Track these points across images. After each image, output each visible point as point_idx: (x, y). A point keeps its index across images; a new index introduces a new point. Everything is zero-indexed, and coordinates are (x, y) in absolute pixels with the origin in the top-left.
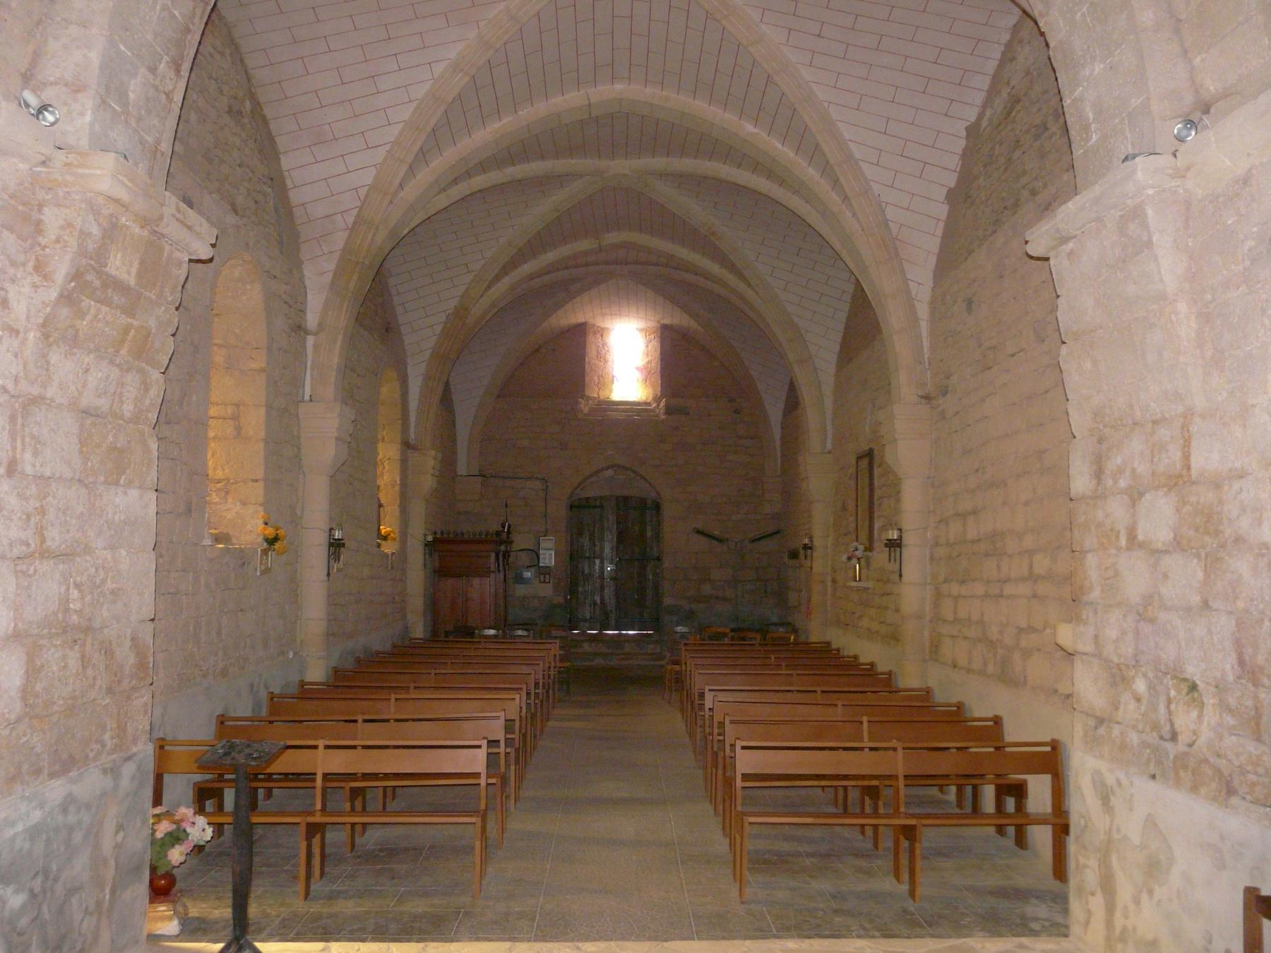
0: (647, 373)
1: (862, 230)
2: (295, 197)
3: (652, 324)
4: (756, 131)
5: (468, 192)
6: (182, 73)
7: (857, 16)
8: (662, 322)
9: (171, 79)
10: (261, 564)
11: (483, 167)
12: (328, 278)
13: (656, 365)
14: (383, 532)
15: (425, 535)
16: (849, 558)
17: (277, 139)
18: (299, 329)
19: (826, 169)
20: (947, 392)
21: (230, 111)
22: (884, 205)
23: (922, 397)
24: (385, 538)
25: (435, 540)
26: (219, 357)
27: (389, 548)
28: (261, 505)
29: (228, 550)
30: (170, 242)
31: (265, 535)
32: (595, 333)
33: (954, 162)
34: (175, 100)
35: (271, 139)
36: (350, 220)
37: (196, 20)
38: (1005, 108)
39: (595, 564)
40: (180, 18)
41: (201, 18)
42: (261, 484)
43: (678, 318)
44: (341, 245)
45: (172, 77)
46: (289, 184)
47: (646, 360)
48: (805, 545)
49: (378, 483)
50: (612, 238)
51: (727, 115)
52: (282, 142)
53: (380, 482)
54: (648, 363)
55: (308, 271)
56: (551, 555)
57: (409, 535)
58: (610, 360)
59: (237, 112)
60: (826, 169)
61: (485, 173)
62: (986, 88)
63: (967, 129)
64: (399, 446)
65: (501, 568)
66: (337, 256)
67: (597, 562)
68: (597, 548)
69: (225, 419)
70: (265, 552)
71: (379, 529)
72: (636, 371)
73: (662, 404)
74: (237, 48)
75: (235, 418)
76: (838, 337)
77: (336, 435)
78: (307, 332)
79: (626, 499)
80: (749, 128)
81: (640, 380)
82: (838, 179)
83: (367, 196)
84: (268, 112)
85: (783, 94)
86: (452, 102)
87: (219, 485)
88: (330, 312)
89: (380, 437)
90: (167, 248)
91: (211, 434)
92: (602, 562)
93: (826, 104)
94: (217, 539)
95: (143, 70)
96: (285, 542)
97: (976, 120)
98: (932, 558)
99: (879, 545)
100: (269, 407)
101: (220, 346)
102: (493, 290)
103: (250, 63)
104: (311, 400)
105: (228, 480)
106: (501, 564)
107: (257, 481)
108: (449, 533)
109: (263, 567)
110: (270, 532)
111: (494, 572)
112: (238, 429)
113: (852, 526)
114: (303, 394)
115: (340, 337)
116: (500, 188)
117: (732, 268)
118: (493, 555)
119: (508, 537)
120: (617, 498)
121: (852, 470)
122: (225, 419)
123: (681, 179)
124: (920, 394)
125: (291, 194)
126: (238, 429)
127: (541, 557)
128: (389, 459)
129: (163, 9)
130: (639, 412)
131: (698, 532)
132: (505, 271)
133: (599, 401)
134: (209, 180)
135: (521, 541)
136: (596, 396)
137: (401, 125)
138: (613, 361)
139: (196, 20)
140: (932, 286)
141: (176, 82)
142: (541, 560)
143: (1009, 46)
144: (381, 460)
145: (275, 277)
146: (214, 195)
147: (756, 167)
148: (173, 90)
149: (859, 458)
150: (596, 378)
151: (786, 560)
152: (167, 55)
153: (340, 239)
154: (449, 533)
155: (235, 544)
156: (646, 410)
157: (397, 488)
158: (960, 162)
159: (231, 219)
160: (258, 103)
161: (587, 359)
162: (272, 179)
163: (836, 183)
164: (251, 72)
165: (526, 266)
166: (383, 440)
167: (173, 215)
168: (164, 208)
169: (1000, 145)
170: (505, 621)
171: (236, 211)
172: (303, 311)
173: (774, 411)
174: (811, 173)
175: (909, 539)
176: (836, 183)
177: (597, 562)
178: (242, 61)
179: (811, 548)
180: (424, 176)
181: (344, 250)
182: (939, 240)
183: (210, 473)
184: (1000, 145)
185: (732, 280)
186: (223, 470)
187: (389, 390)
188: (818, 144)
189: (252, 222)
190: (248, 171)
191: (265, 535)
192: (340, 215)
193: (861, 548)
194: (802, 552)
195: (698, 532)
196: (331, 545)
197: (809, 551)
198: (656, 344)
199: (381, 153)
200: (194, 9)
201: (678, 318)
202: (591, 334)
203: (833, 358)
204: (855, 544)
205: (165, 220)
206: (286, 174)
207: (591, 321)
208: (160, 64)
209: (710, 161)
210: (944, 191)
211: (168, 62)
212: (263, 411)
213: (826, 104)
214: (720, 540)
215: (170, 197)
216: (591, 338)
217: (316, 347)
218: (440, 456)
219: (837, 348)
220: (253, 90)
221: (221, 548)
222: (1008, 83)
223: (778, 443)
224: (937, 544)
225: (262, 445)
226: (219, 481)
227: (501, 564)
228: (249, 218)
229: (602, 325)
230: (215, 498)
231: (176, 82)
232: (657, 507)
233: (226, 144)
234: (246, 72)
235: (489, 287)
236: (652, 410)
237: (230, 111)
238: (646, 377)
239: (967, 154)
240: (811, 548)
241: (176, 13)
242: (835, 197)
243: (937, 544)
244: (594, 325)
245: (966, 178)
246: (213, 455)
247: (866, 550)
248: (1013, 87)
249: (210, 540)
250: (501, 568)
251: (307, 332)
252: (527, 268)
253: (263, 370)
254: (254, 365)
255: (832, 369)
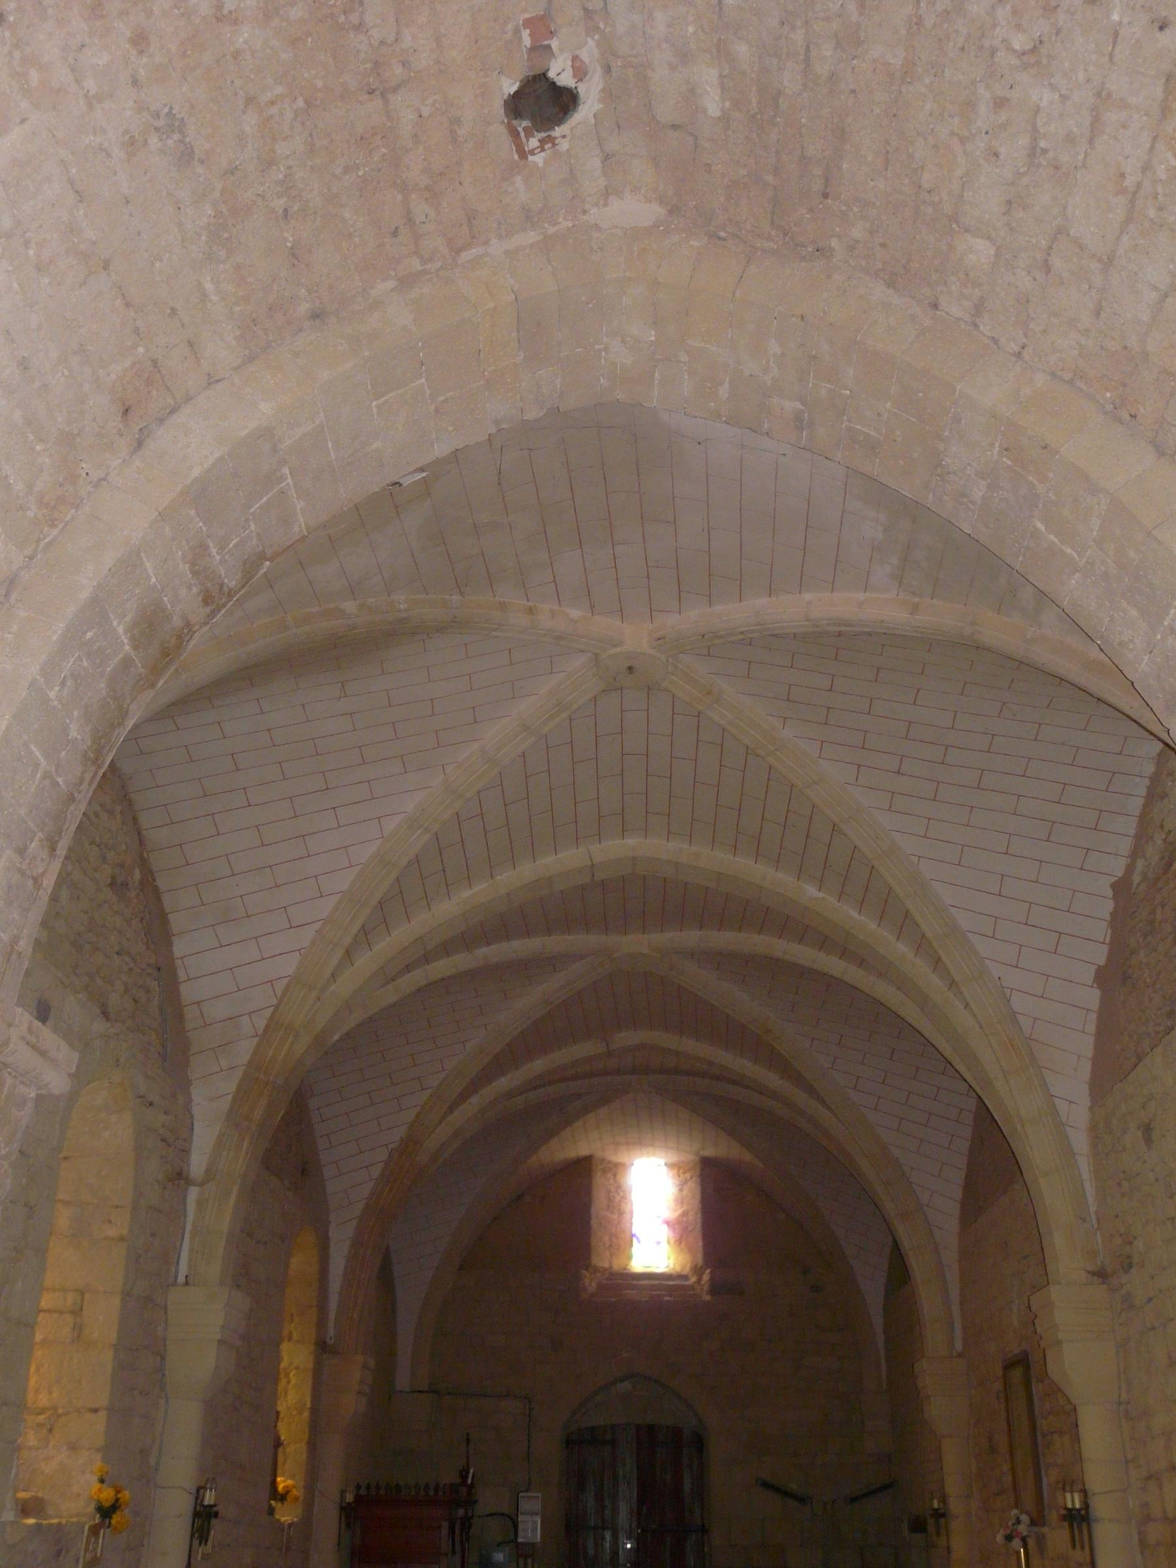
0: (681, 1230)
1: (980, 1028)
2: (187, 992)
3: (688, 1157)
4: (821, 895)
5: (423, 983)
6: (58, 852)
7: (947, 747)
8: (702, 1153)
9: (42, 860)
10: (86, 1550)
11: (447, 948)
12: (225, 1104)
13: (695, 1218)
14: (281, 1487)
15: (343, 1493)
16: (1009, 1538)
17: (171, 917)
18: (179, 1177)
19: (922, 945)
20: (1130, 1266)
21: (112, 885)
22: (1008, 991)
23: (1093, 1274)
24: (282, 1498)
25: (358, 1498)
26: (63, 1219)
27: (286, 1515)
28: (98, 1450)
29: (38, 1526)
30: (13, 1074)
31: (99, 1501)
32: (604, 1171)
33: (1101, 930)
34: (45, 884)
35: (163, 917)
36: (261, 1024)
37: (84, 786)
38: (1162, 858)
39: (603, 1538)
40: (64, 787)
41: (90, 785)
42: (103, 1414)
43: (723, 1148)
44: (245, 1058)
45: (44, 857)
46: (181, 974)
47: (680, 1211)
48: (936, 1510)
49: (279, 1408)
50: (625, 1038)
51: (780, 875)
52: (176, 922)
53: (281, 1407)
54: (684, 1214)
55: (198, 1094)
56: (535, 1522)
57: (317, 1492)
58: (627, 1211)
59: (122, 884)
60: (922, 945)
61: (448, 955)
62: (1132, 832)
63: (1114, 886)
64: (312, 1348)
65: (457, 1548)
66: (238, 1074)
67: (608, 1535)
68: (607, 1512)
69: (61, 1313)
70: (95, 1531)
71: (274, 1483)
72: (665, 1226)
73: (706, 1277)
74: (130, 804)
75: (77, 1311)
76: (959, 1177)
77: (218, 1337)
78: (189, 1182)
79: (651, 1429)
80: (811, 891)
81: (672, 1241)
82: (939, 959)
83: (285, 991)
84: (162, 883)
85: (855, 847)
86: (406, 867)
87: (41, 1418)
88: (225, 1153)
89: (285, 1333)
90: (9, 1081)
91: (38, 1337)
92: (615, 1537)
93: (915, 859)
94: (25, 1509)
95: (9, 852)
96: (127, 1511)
97: (1125, 874)
98: (1143, 1543)
99: (1053, 1516)
100: (126, 1295)
101: (67, 1203)
102: (456, 1113)
103: (144, 820)
104: (187, 1283)
105: (55, 1408)
106: (457, 1544)
107: (96, 1411)
108: (378, 1487)
109: (89, 1556)
110: (107, 1495)
111: (446, 1555)
112: (78, 1330)
113: (1008, 1480)
114: (177, 1272)
115: (235, 1189)
116: (471, 975)
117: (798, 1079)
118: (445, 1524)
119: (469, 1494)
120: (638, 1427)
121: (998, 1386)
122: (61, 1313)
123: (719, 960)
124: (1089, 1268)
125: (184, 989)
126: (78, 1330)
127: (521, 1526)
128: (297, 1368)
129: (44, 778)
130: (671, 1290)
131: (767, 1485)
132: (474, 1086)
133: (611, 1274)
134: (76, 975)
135: (489, 1500)
136: (606, 1265)
137: (337, 898)
138: (631, 1212)
139: (84, 786)
140: (1090, 1104)
141: (48, 865)
142: (520, 1533)
143: (1155, 779)
144: (285, 1369)
145: (151, 1104)
146: (80, 996)
147: (824, 943)
148: (43, 874)
149: (1008, 1366)
150: (606, 1238)
151: (906, 1533)
152: (42, 830)
153: (244, 1051)
154: (378, 1487)
155: (50, 1517)
156: (683, 1287)
157: (306, 1414)
158: (1110, 931)
159: (99, 1026)
160: (151, 872)
161: (593, 1211)
162: (159, 969)
163: (937, 963)
164: (144, 832)
165: (503, 1079)
166: (290, 1338)
167: (23, 1038)
168: (12, 1029)
169: (1163, 907)
170: (379, 1118)
171: (105, 1015)
172: (186, 1152)
173: (872, 1289)
174: (901, 950)
175: (1102, 1508)
176: (937, 963)
177: (608, 1535)
178: (135, 819)
179: (943, 1515)
180: (366, 962)
181: (250, 1063)
182: (1092, 1039)
183: (30, 1397)
184: (1163, 907)
185: (800, 1097)
186: (50, 1393)
187: (301, 1262)
188: (908, 911)
189: (128, 1028)
190: (128, 959)
191: (99, 1501)
192: (246, 1018)
193: (1025, 1518)
194: (931, 1521)
195: (767, 1485)
196: (196, 1514)
197: (942, 1521)
198: (694, 1187)
199: (309, 933)
200: (83, 773)
201: (723, 1148)
202: (599, 1174)
203: (954, 1209)
204: (1015, 1512)
205: (11, 1046)
206: (178, 963)
207: (598, 1154)
208: (31, 843)
209: (760, 933)
210: (1092, 970)
211: (41, 840)
212: (116, 1301)
213: (915, 859)
214: (801, 1500)
215: (22, 1014)
216: (599, 1180)
217: (200, 1204)
218: (372, 1363)
219: (958, 1193)
220: (145, 855)
221: (29, 1526)
222: (1162, 827)
223: (880, 1340)
224: (1148, 1519)
225: (108, 1356)
226: (42, 1411)
227: (457, 1544)
228: (124, 1022)
229: (615, 1158)
230: (31, 1439)
231: (48, 865)
232: (700, 1442)
233: (103, 926)
234: (139, 834)
235: (451, 1109)
236: (691, 1287)
237: (112, 885)
238: (681, 1237)
239: (1117, 920)
240: (943, 1515)
241: (60, 780)
242: (935, 980)
243: (1148, 1519)
244: (603, 1160)
245: (1120, 953)
246: (38, 1370)
247: (1033, 1523)
248: (1170, 832)
249: (13, 1513)
250: (457, 1548)
251: (189, 1182)
252: (504, 1083)
253: (122, 1239)
254: (111, 1232)
255: (954, 1225)
